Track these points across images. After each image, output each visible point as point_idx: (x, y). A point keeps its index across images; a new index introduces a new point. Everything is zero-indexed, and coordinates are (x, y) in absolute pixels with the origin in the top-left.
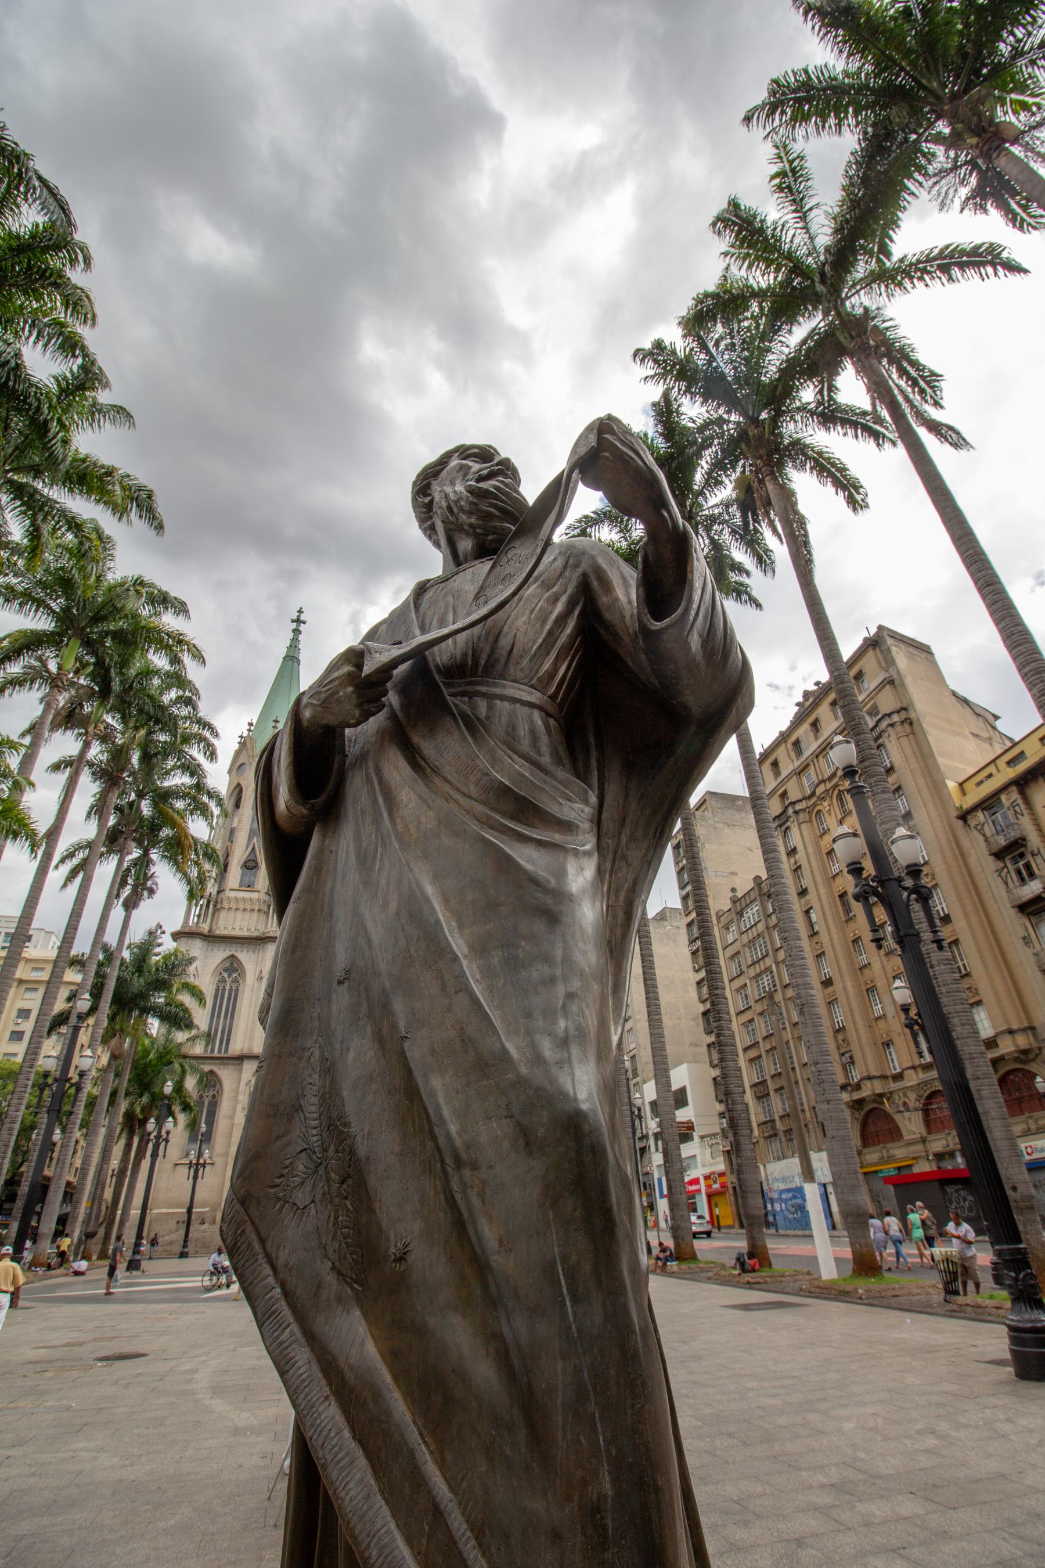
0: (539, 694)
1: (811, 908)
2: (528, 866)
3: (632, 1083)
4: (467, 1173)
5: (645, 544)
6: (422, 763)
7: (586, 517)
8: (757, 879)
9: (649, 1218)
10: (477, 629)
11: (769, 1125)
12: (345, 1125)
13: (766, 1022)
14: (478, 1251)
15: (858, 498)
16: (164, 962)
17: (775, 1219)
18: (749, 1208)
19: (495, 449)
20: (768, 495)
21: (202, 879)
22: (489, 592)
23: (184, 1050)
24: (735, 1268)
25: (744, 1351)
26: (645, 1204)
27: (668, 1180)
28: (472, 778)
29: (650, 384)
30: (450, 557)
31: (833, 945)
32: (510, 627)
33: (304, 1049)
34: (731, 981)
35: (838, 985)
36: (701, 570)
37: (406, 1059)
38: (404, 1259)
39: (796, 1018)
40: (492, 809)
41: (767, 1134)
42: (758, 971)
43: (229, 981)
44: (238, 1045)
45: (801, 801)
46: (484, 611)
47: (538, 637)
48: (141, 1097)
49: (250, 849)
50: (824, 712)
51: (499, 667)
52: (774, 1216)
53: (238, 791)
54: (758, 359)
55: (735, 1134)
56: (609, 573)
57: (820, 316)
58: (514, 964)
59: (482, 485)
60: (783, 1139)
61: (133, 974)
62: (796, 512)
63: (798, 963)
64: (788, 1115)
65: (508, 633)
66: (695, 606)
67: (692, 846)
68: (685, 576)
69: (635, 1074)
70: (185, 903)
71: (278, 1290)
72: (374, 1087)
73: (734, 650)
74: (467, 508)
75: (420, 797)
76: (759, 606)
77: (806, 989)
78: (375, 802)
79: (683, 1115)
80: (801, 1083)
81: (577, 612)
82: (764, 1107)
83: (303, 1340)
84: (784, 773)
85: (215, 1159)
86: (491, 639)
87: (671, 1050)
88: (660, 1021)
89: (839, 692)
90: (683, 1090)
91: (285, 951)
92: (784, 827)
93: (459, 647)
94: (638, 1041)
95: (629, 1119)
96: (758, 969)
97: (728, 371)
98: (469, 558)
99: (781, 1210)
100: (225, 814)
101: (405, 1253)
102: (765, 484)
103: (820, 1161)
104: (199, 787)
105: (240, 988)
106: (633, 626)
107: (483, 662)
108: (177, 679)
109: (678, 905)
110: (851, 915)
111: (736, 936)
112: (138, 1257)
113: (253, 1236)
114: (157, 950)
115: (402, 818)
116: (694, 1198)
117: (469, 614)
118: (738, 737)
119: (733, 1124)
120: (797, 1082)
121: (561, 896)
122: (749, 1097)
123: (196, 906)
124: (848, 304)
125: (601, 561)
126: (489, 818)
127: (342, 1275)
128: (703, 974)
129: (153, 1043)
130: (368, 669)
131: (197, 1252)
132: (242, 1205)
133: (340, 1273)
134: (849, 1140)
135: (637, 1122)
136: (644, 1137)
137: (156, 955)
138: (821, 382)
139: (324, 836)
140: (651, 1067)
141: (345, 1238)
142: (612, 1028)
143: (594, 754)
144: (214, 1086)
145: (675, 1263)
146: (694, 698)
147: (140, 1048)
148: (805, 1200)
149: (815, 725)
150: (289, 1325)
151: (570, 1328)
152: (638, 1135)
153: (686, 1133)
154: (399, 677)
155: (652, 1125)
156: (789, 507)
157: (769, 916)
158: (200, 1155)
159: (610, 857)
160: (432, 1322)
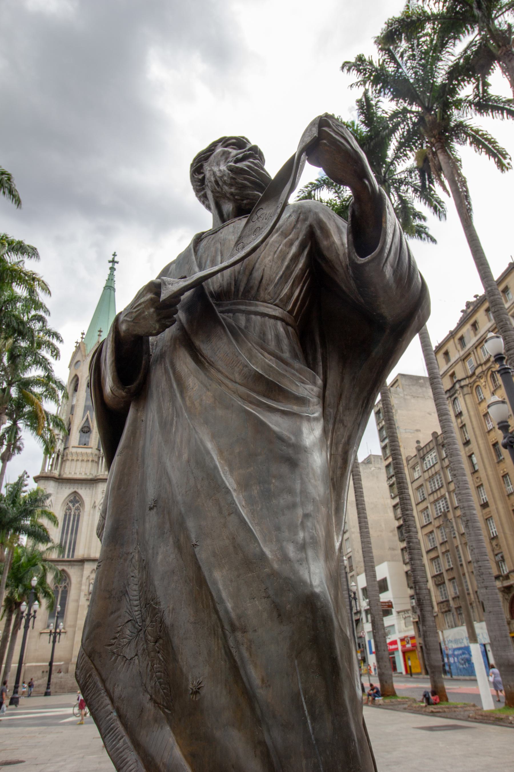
0: (281, 310)
1: (473, 454)
2: (276, 428)
3: (349, 575)
4: (239, 634)
5: (353, 204)
6: (203, 359)
7: (311, 184)
8: (434, 434)
9: (362, 667)
10: (237, 267)
11: (445, 604)
12: (156, 604)
13: (442, 533)
14: (248, 686)
15: (505, 162)
16: (30, 497)
17: (450, 668)
18: (433, 662)
19: (247, 139)
20: (440, 163)
21: (52, 441)
22: (245, 240)
23: (45, 556)
24: (422, 702)
25: (430, 759)
26: (360, 658)
27: (375, 641)
28: (237, 369)
29: (355, 88)
30: (217, 216)
31: (488, 479)
32: (260, 264)
33: (128, 554)
34: (417, 504)
35: (492, 507)
36: (392, 221)
37: (197, 559)
38: (199, 692)
39: (463, 530)
40: (251, 390)
41: (443, 610)
42: (436, 498)
43: (73, 509)
44: (80, 553)
45: (464, 379)
46: (242, 254)
47: (279, 271)
48: (17, 587)
49: (85, 419)
50: (481, 316)
51: (253, 292)
52: (450, 666)
53: (75, 380)
54: (432, 66)
55: (421, 610)
56: (328, 224)
57: (476, 32)
58: (268, 495)
59: (239, 165)
60: (455, 613)
61: (9, 505)
62: (460, 175)
63: (464, 492)
64: (458, 597)
65: (259, 268)
66: (388, 246)
67: (388, 412)
68: (381, 225)
69: (351, 570)
70: (43, 456)
71: (115, 714)
72: (176, 578)
73: (416, 276)
74: (229, 181)
75: (202, 383)
76: (434, 240)
77: (469, 509)
78: (171, 386)
79: (384, 597)
80: (467, 575)
81: (306, 253)
82: (441, 592)
83: (132, 747)
84: (453, 359)
85: (67, 629)
86: (247, 273)
87: (376, 552)
88: (368, 532)
89: (491, 302)
90: (384, 580)
91: (113, 488)
92: (453, 398)
93: (225, 279)
94: (353, 547)
95: (347, 600)
96: (435, 496)
97: (410, 75)
98: (231, 216)
99: (454, 662)
100: (66, 396)
101: (199, 689)
102: (437, 156)
103: (481, 629)
104: (49, 378)
105: (81, 514)
106: (345, 261)
107: (242, 289)
108: (33, 302)
109: (380, 453)
110: (501, 458)
111: (420, 474)
112: (17, 696)
113: (97, 678)
114: (24, 489)
115: (190, 397)
116: (393, 654)
117: (232, 256)
118: (420, 335)
119: (420, 603)
120: (464, 574)
121: (299, 448)
122: (431, 584)
123: (50, 458)
124: (496, 22)
125: (322, 216)
126: (249, 396)
127: (157, 703)
128: (397, 500)
129: (24, 552)
130: (164, 296)
131: (56, 692)
132: (90, 657)
133: (155, 702)
134: (501, 614)
135: (353, 602)
136: (359, 612)
137: (24, 492)
138: (477, 80)
139: (137, 410)
140: (362, 564)
141: (158, 679)
142: (335, 538)
143: (319, 350)
144: (65, 580)
145: (381, 698)
146: (389, 311)
147: (15, 555)
148: (471, 656)
149: (475, 326)
150: (122, 737)
151: (311, 738)
152: (354, 611)
153: (387, 609)
154: (185, 300)
155: (363, 604)
156: (455, 171)
157: (443, 459)
158: (57, 626)
159: (332, 421)
160: (218, 734)
